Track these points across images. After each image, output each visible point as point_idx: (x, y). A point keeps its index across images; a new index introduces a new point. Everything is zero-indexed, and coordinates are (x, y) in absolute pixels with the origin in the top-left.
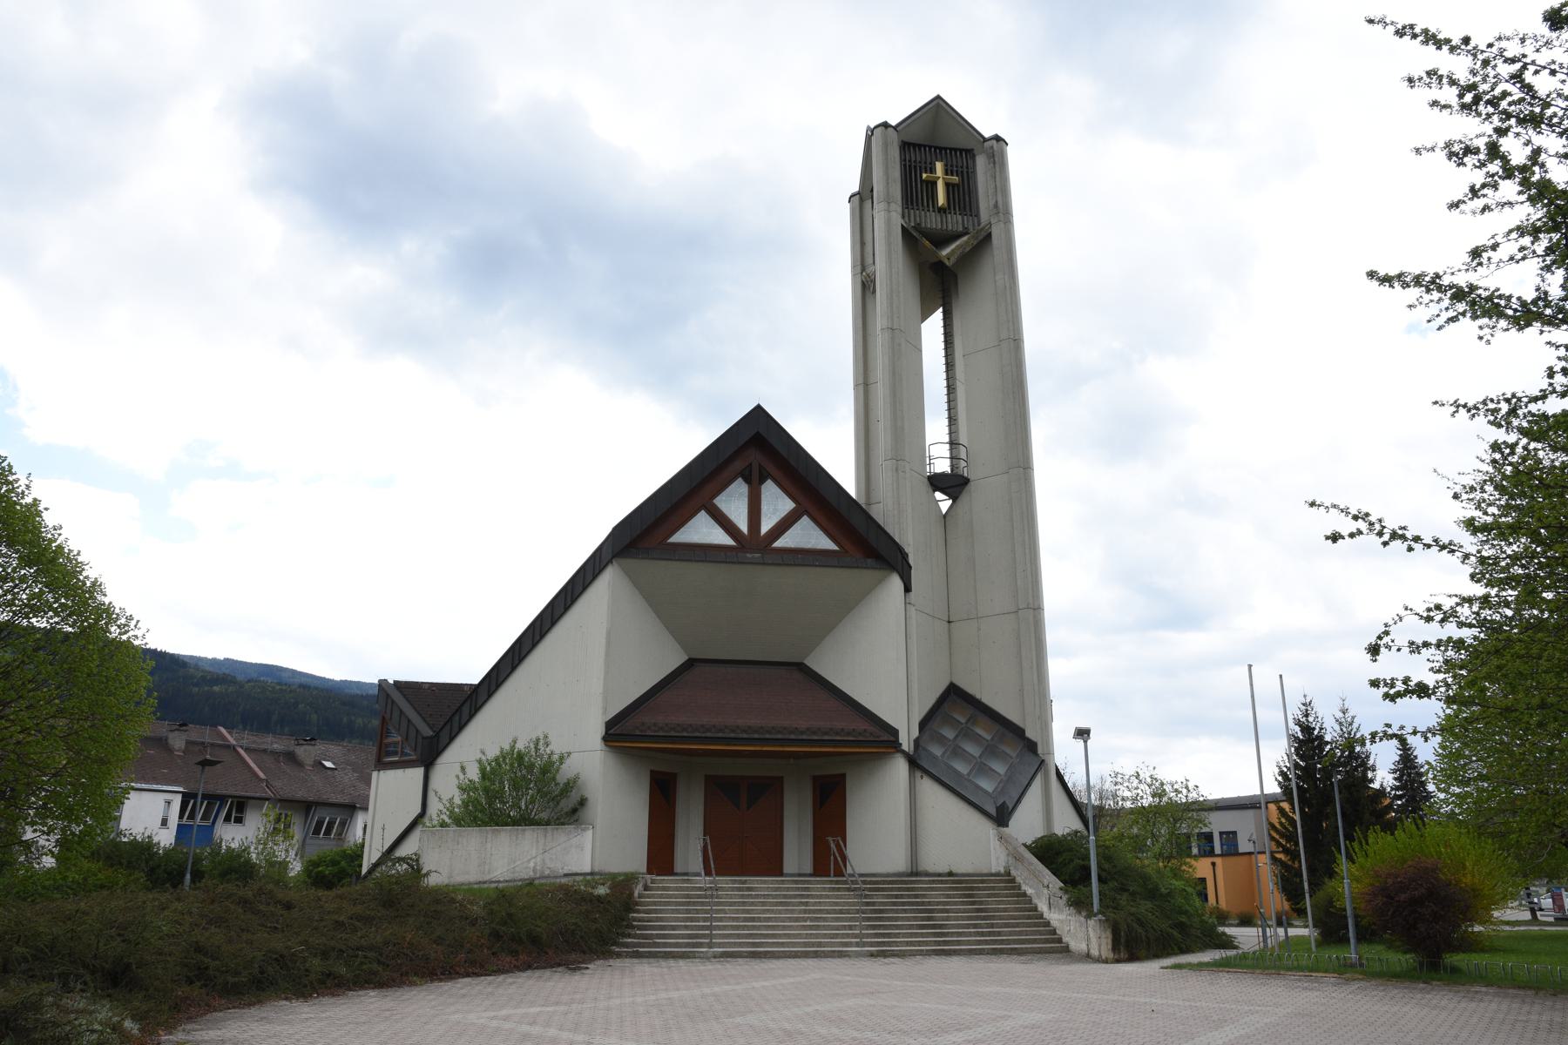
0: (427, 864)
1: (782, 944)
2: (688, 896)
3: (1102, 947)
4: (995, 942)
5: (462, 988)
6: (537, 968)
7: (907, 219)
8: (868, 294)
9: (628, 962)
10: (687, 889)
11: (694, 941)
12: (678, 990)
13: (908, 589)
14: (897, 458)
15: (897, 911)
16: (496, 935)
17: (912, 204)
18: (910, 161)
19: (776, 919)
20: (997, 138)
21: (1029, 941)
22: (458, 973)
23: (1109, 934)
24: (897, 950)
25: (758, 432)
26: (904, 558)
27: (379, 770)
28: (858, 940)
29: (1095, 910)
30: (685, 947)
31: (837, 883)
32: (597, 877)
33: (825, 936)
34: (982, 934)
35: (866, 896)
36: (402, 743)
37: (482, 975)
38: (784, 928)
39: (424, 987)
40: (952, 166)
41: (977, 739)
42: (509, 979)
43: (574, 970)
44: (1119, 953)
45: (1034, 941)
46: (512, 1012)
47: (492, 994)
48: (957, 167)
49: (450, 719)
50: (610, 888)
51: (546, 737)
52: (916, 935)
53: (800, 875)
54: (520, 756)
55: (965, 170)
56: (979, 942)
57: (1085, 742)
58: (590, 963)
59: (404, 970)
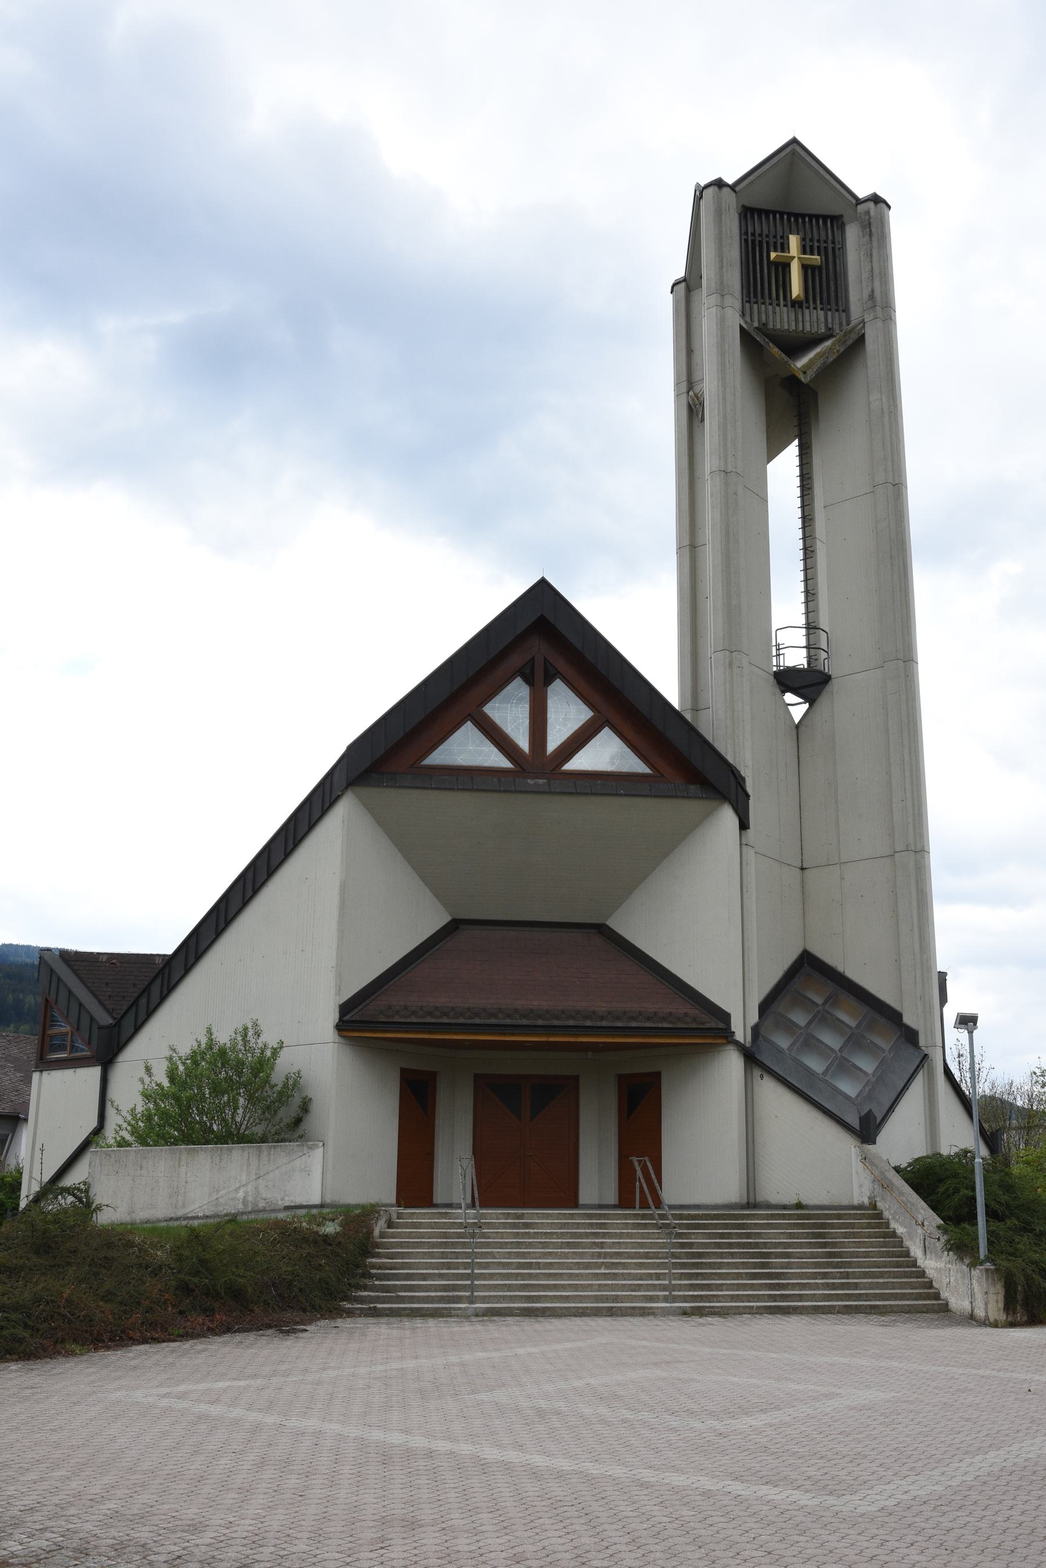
0: (100, 1195)
1: (567, 1299)
2: (445, 1235)
3: (990, 1306)
4: (849, 1297)
5: (133, 1359)
6: (238, 1331)
7: (748, 319)
8: (696, 422)
9: (360, 1322)
10: (444, 1225)
11: (451, 1294)
12: (416, 1358)
13: (744, 825)
14: (731, 649)
15: (721, 1255)
16: (185, 1289)
17: (755, 296)
18: (753, 234)
19: (560, 1265)
20: (876, 199)
21: (895, 1297)
22: (131, 1338)
23: (1000, 1288)
24: (718, 1307)
25: (542, 615)
26: (739, 783)
27: (41, 1071)
28: (667, 1293)
29: (982, 1257)
30: (438, 1303)
31: (644, 1217)
32: (325, 1211)
33: (623, 1287)
34: (834, 1286)
35: (679, 1235)
36: (72, 1034)
37: (164, 1341)
38: (571, 1276)
39: (85, 1357)
40: (811, 240)
41: (838, 1026)
42: (199, 1345)
43: (288, 1332)
44: (1015, 1313)
45: (903, 1297)
46: (192, 1387)
47: (173, 1364)
48: (818, 241)
49: (136, 1003)
50: (341, 1225)
51: (255, 1024)
52: (744, 1287)
53: (601, 1207)
54: (223, 1052)
55: (830, 246)
56: (828, 1298)
57: (971, 1033)
58: (310, 1324)
59: (60, 1334)
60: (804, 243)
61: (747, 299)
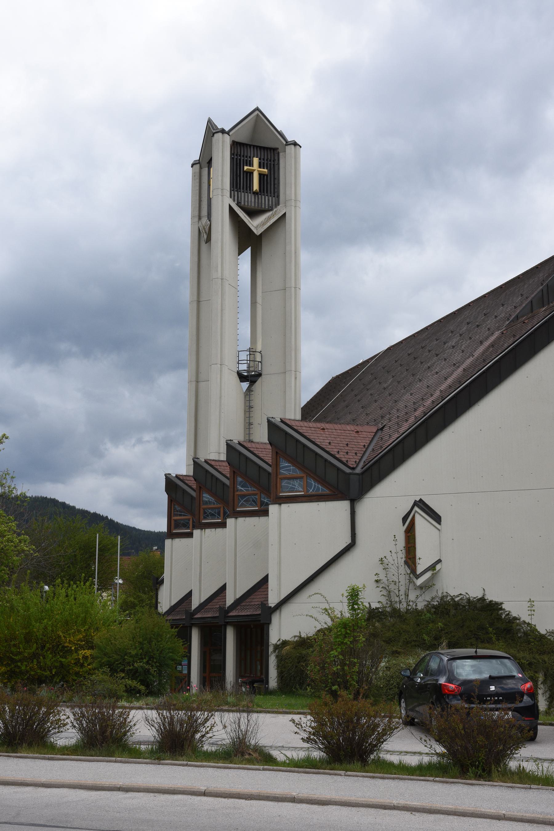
27: (236, 518)
48: (237, 155)
55: (272, 163)
60: (260, 161)
61: (274, 195)
